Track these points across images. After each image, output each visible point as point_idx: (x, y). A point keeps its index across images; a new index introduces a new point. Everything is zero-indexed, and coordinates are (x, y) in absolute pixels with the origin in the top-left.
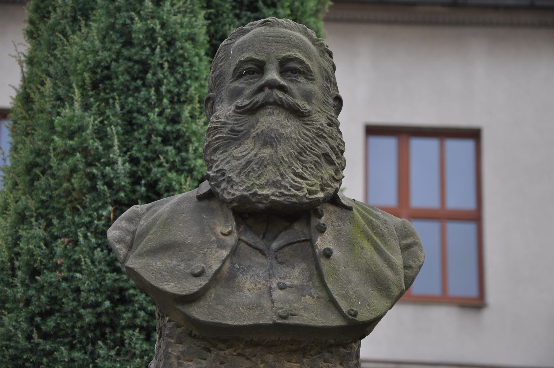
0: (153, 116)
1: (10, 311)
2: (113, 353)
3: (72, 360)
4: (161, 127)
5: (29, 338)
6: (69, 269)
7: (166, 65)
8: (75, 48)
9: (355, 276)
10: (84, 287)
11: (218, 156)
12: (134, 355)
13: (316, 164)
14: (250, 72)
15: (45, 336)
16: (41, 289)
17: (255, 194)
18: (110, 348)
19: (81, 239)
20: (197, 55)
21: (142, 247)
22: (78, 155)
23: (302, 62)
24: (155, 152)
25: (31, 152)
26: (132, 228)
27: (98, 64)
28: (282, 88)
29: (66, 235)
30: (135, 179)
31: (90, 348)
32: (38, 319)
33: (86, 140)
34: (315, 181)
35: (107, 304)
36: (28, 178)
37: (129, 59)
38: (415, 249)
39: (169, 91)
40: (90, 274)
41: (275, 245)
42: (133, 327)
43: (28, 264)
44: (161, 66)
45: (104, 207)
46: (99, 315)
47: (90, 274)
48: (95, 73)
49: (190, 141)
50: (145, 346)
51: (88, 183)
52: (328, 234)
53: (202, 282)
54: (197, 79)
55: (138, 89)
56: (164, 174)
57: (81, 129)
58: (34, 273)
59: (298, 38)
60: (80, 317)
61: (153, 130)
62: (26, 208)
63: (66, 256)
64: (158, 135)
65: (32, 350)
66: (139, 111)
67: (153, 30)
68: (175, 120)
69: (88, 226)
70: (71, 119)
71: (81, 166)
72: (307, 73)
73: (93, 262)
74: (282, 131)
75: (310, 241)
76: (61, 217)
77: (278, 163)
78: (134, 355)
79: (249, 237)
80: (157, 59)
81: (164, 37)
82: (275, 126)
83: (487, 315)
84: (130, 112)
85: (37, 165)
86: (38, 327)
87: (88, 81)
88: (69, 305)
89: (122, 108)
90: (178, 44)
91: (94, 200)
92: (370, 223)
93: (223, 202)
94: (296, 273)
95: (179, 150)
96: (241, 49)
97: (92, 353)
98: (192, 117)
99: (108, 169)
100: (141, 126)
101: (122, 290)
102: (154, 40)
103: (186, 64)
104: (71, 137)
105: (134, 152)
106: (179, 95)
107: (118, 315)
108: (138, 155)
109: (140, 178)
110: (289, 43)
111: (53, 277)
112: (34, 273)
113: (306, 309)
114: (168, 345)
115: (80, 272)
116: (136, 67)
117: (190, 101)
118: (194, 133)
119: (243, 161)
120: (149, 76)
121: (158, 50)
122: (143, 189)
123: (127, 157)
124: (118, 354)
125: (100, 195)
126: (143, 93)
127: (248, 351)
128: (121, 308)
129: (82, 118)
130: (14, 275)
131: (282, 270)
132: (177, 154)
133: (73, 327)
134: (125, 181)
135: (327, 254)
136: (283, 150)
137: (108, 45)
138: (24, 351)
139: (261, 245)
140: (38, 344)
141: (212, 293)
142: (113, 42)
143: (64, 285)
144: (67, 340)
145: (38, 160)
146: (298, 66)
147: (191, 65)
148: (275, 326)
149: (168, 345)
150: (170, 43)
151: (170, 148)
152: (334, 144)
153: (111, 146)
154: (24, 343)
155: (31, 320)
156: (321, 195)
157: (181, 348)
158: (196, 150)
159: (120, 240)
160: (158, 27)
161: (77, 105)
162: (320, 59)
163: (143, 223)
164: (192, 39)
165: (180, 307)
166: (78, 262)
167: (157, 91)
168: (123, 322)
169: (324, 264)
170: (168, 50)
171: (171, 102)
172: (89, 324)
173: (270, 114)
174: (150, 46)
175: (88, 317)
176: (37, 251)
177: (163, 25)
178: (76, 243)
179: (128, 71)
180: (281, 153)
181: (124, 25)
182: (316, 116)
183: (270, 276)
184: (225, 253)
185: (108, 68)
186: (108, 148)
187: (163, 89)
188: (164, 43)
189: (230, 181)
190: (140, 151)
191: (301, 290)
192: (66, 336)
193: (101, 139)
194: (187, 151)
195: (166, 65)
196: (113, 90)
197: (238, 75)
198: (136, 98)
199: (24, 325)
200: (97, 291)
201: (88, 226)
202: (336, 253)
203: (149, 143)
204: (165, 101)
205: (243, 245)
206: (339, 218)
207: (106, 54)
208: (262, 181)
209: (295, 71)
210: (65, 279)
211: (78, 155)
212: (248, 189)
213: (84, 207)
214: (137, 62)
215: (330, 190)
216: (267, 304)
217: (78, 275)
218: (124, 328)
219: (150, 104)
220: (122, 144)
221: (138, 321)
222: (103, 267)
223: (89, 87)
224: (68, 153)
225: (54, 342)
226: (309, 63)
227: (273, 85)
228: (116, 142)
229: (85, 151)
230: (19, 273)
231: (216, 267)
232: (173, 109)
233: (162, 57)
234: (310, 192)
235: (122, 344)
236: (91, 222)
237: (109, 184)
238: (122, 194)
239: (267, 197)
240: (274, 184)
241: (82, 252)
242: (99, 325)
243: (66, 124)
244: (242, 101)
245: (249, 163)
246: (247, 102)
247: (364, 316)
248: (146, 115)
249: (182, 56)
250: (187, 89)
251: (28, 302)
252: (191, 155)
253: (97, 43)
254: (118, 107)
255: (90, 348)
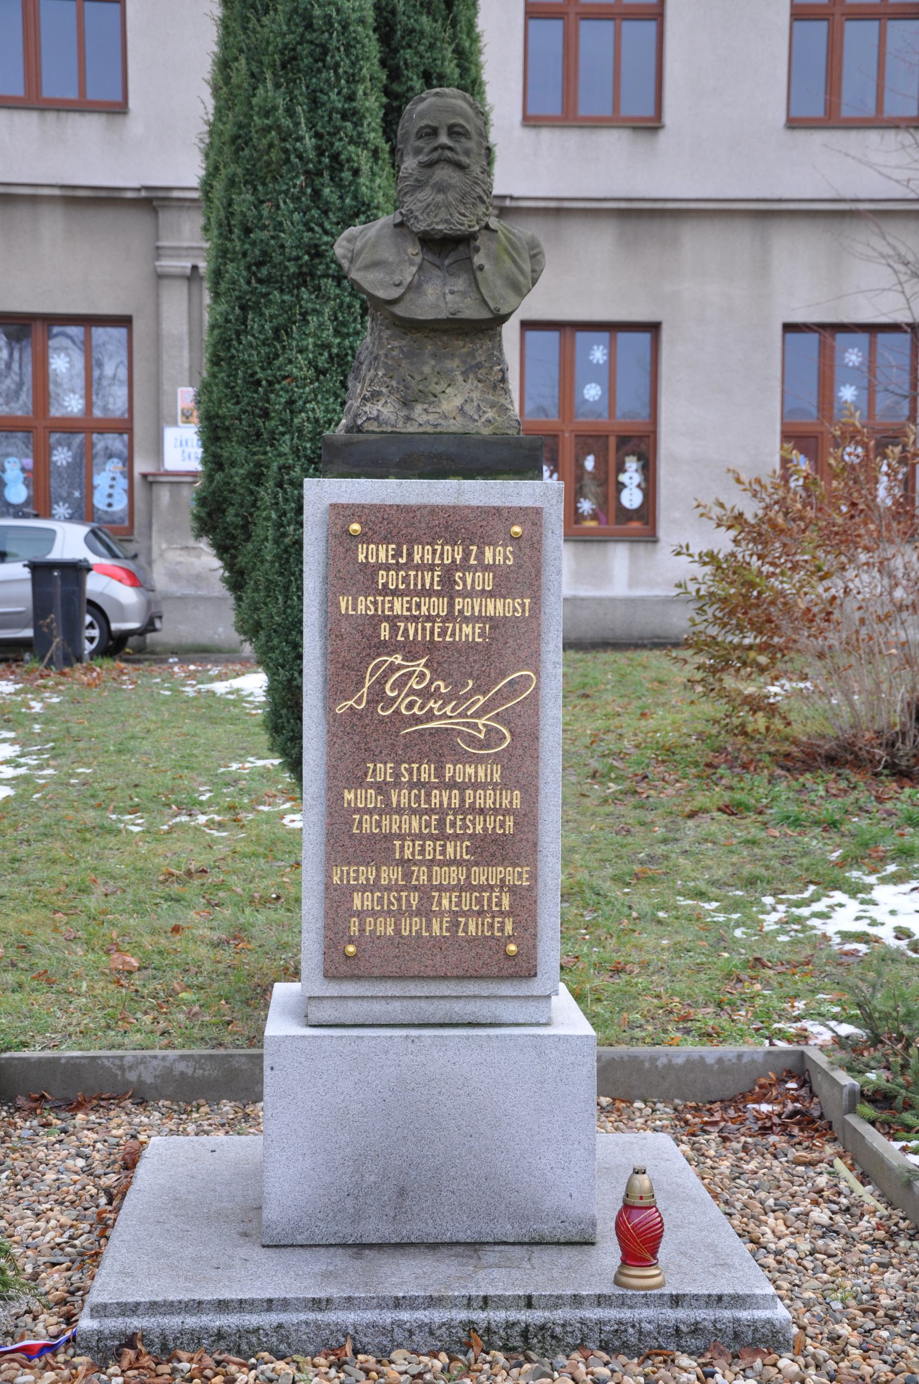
0: (333, 96)
1: (232, 261)
2: (313, 297)
3: (283, 301)
4: (340, 106)
5: (249, 283)
6: (275, 230)
7: (342, 49)
8: (266, 30)
9: (499, 282)
10: (288, 244)
11: (408, 199)
12: (329, 298)
13: (474, 204)
14: (427, 134)
15: (260, 281)
16: (254, 244)
17: (433, 229)
18: (311, 293)
19: (282, 205)
20: (367, 36)
21: (360, 263)
22: (273, 133)
23: (463, 127)
24: (336, 127)
25: (234, 124)
26: (351, 247)
27: (285, 46)
28: (450, 149)
29: (269, 200)
30: (320, 152)
31: (295, 292)
32: (254, 268)
33: (278, 119)
34: (472, 217)
35: (306, 257)
36: (233, 148)
37: (311, 42)
38: (539, 257)
39: (345, 72)
40: (291, 234)
41: (447, 262)
42: (327, 276)
43: (241, 222)
44: (338, 49)
45: (297, 177)
46: (301, 266)
47: (291, 234)
48: (283, 54)
49: (364, 117)
50: (338, 291)
51: (283, 156)
52: (481, 253)
53: (400, 291)
54: (368, 59)
55: (319, 71)
56: (344, 148)
57: (275, 108)
58: (247, 231)
59: (461, 107)
60: (286, 268)
61: (333, 108)
62: (234, 175)
63: (271, 218)
64: (337, 112)
65: (251, 292)
66: (321, 91)
67: (330, 16)
68: (351, 98)
69: (286, 192)
70: (265, 99)
71: (276, 142)
72: (466, 134)
73: (292, 223)
74: (450, 181)
75: (470, 259)
76: (264, 184)
77: (448, 206)
78: (329, 298)
79: (429, 257)
80: (334, 43)
81: (340, 22)
82: (446, 178)
83: (662, 135)
84: (314, 91)
85: (239, 137)
86: (254, 274)
87: (278, 63)
88: (277, 258)
89: (307, 87)
90: (352, 28)
91: (289, 171)
92: (509, 240)
93: (412, 232)
94: (461, 281)
95: (355, 125)
96: (421, 116)
97: (297, 296)
98: (365, 94)
99: (298, 144)
100: (323, 104)
101: (316, 246)
102: (332, 25)
103: (358, 46)
104: (267, 117)
105: (319, 128)
106: (353, 75)
107: (315, 267)
108: (322, 131)
109: (324, 151)
110: (454, 111)
111: (264, 235)
112: (247, 231)
113: (467, 307)
114: (381, 331)
115: (283, 231)
116: (318, 50)
117: (363, 80)
118: (367, 109)
119: (424, 204)
120: (328, 58)
121: (335, 34)
122: (327, 160)
123: (312, 133)
124: (317, 297)
125: (293, 168)
126: (324, 75)
127: (431, 334)
128: (317, 261)
129: (274, 98)
130: (231, 232)
131: (452, 280)
132: (354, 129)
133: (282, 276)
134: (312, 155)
135: (481, 268)
136: (451, 196)
137: (293, 28)
138: (246, 293)
139: (438, 262)
140: (256, 288)
141: (408, 297)
142: (297, 25)
143: (272, 242)
144: (277, 285)
145: (241, 132)
146: (460, 130)
147: (363, 46)
148: (448, 320)
149: (381, 331)
150: (345, 27)
151: (348, 124)
152: (485, 188)
153: (299, 123)
154: (245, 287)
155: (248, 268)
156: (477, 228)
157: (389, 332)
158: (369, 125)
159: (344, 257)
160: (334, 14)
161: (269, 85)
162: (476, 119)
163: (359, 244)
164: (362, 21)
165: (387, 307)
166: (281, 224)
167: (336, 72)
168: (319, 273)
169: (479, 275)
170: (343, 34)
171: (348, 81)
172: (294, 274)
173: (443, 168)
174: (328, 31)
175: (292, 268)
176: (249, 213)
177: (338, 11)
178: (278, 207)
179: (311, 54)
180: (451, 199)
181: (306, 9)
182: (473, 167)
183: (444, 285)
184: (414, 269)
185: (294, 49)
186: (297, 124)
187: (341, 71)
188: (339, 28)
189: (416, 218)
190: (323, 127)
191: (464, 294)
192: (277, 282)
193: (291, 116)
194: (362, 125)
195: (342, 49)
196: (299, 71)
197: (419, 136)
198: (319, 79)
199: (244, 273)
200: (297, 247)
201: (286, 192)
202: (487, 267)
203: (330, 119)
204: (343, 82)
205: (426, 263)
206: (489, 240)
207: (292, 36)
208: (438, 219)
209: (458, 133)
210: (273, 237)
211: (273, 133)
212: (429, 225)
213: (282, 177)
214: (317, 45)
215: (483, 224)
216: (443, 305)
217: (282, 235)
218: (320, 277)
219: (329, 85)
220: (308, 120)
221: (331, 272)
222: (301, 227)
223: (278, 68)
224: (266, 130)
225: (268, 286)
226: (468, 127)
227: (444, 147)
228: (303, 120)
229: (279, 128)
230: (236, 230)
231: (409, 279)
232: (349, 88)
233: (338, 41)
234: (470, 227)
235: (319, 289)
236: (288, 190)
237: (300, 157)
238: (311, 166)
239: (441, 231)
240: (446, 221)
241: (284, 215)
242: (301, 274)
243: (262, 104)
244: (422, 158)
245: (428, 205)
246: (426, 159)
247: (504, 311)
248: (327, 94)
249: (355, 38)
250: (361, 69)
251: (245, 254)
252: (365, 129)
253: (285, 28)
254: (304, 88)
255: (295, 292)
